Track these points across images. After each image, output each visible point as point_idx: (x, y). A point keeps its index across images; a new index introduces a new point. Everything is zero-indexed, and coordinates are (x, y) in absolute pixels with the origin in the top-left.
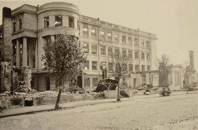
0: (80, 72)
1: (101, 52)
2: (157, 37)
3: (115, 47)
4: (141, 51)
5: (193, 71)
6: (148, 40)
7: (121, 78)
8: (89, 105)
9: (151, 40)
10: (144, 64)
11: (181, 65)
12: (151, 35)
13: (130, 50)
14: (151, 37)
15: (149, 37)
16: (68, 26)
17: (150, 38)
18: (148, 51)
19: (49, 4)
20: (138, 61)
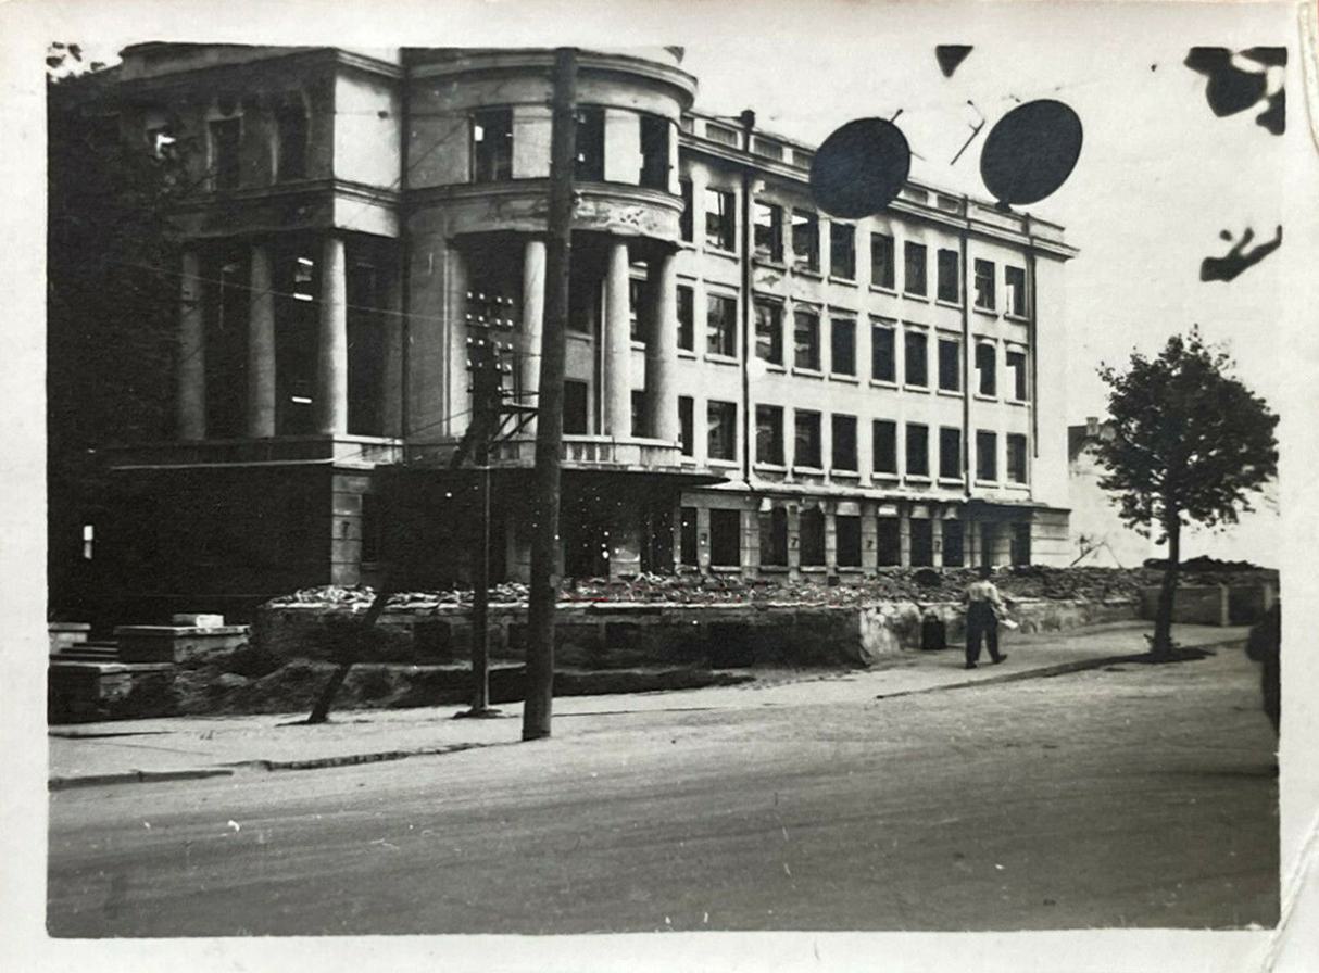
0: (500, 527)
1: (709, 337)
2: (1068, 238)
3: (832, 309)
4: (979, 337)
5: (470, 326)
6: (1019, 262)
7: (1004, 553)
8: (1221, 650)
9: (1034, 265)
10: (988, 427)
11: (71, 73)
12: (1035, 229)
13: (915, 329)
14: (1036, 243)
15: (1025, 240)
16: (635, 179)
17: (1031, 253)
18: (1019, 334)
19: (642, 61)
20: (960, 403)
